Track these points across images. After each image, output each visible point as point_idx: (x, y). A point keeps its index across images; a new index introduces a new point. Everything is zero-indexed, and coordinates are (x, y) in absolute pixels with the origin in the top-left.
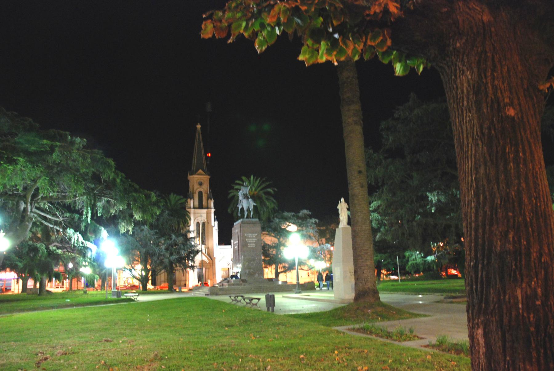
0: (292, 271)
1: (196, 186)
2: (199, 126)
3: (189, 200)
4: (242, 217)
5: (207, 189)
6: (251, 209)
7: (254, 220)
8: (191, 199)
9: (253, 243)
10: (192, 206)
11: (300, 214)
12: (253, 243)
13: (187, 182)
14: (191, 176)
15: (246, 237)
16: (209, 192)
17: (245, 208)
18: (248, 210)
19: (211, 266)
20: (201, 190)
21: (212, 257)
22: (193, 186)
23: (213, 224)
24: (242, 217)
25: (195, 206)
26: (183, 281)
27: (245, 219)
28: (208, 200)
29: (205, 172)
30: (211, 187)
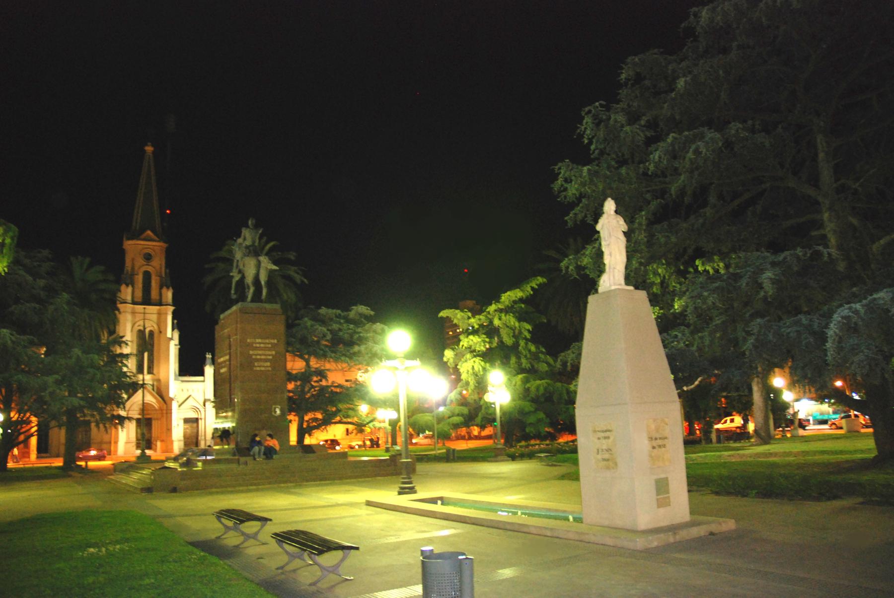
0: (328, 428)
1: (140, 261)
2: (149, 149)
3: (123, 287)
4: (242, 298)
5: (161, 268)
6: (263, 279)
7: (268, 306)
8: (127, 285)
9: (266, 360)
10: (129, 298)
11: (352, 314)
12: (266, 360)
13: (122, 253)
14: (130, 242)
15: (251, 346)
16: (164, 276)
17: (249, 279)
18: (257, 281)
19: (162, 414)
20: (149, 269)
21: (166, 399)
22: (133, 260)
23: (169, 335)
24: (242, 298)
25: (136, 300)
26: (106, 443)
27: (249, 305)
28: (161, 288)
29: (158, 238)
30: (168, 264)
